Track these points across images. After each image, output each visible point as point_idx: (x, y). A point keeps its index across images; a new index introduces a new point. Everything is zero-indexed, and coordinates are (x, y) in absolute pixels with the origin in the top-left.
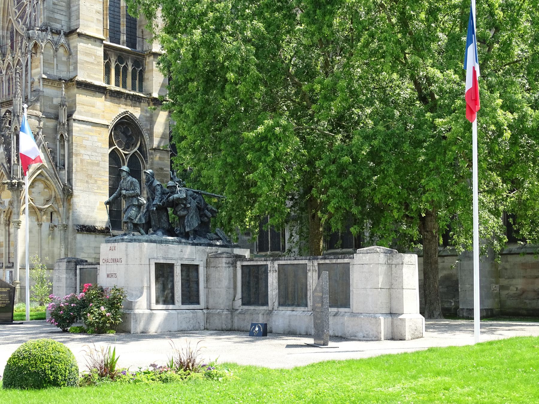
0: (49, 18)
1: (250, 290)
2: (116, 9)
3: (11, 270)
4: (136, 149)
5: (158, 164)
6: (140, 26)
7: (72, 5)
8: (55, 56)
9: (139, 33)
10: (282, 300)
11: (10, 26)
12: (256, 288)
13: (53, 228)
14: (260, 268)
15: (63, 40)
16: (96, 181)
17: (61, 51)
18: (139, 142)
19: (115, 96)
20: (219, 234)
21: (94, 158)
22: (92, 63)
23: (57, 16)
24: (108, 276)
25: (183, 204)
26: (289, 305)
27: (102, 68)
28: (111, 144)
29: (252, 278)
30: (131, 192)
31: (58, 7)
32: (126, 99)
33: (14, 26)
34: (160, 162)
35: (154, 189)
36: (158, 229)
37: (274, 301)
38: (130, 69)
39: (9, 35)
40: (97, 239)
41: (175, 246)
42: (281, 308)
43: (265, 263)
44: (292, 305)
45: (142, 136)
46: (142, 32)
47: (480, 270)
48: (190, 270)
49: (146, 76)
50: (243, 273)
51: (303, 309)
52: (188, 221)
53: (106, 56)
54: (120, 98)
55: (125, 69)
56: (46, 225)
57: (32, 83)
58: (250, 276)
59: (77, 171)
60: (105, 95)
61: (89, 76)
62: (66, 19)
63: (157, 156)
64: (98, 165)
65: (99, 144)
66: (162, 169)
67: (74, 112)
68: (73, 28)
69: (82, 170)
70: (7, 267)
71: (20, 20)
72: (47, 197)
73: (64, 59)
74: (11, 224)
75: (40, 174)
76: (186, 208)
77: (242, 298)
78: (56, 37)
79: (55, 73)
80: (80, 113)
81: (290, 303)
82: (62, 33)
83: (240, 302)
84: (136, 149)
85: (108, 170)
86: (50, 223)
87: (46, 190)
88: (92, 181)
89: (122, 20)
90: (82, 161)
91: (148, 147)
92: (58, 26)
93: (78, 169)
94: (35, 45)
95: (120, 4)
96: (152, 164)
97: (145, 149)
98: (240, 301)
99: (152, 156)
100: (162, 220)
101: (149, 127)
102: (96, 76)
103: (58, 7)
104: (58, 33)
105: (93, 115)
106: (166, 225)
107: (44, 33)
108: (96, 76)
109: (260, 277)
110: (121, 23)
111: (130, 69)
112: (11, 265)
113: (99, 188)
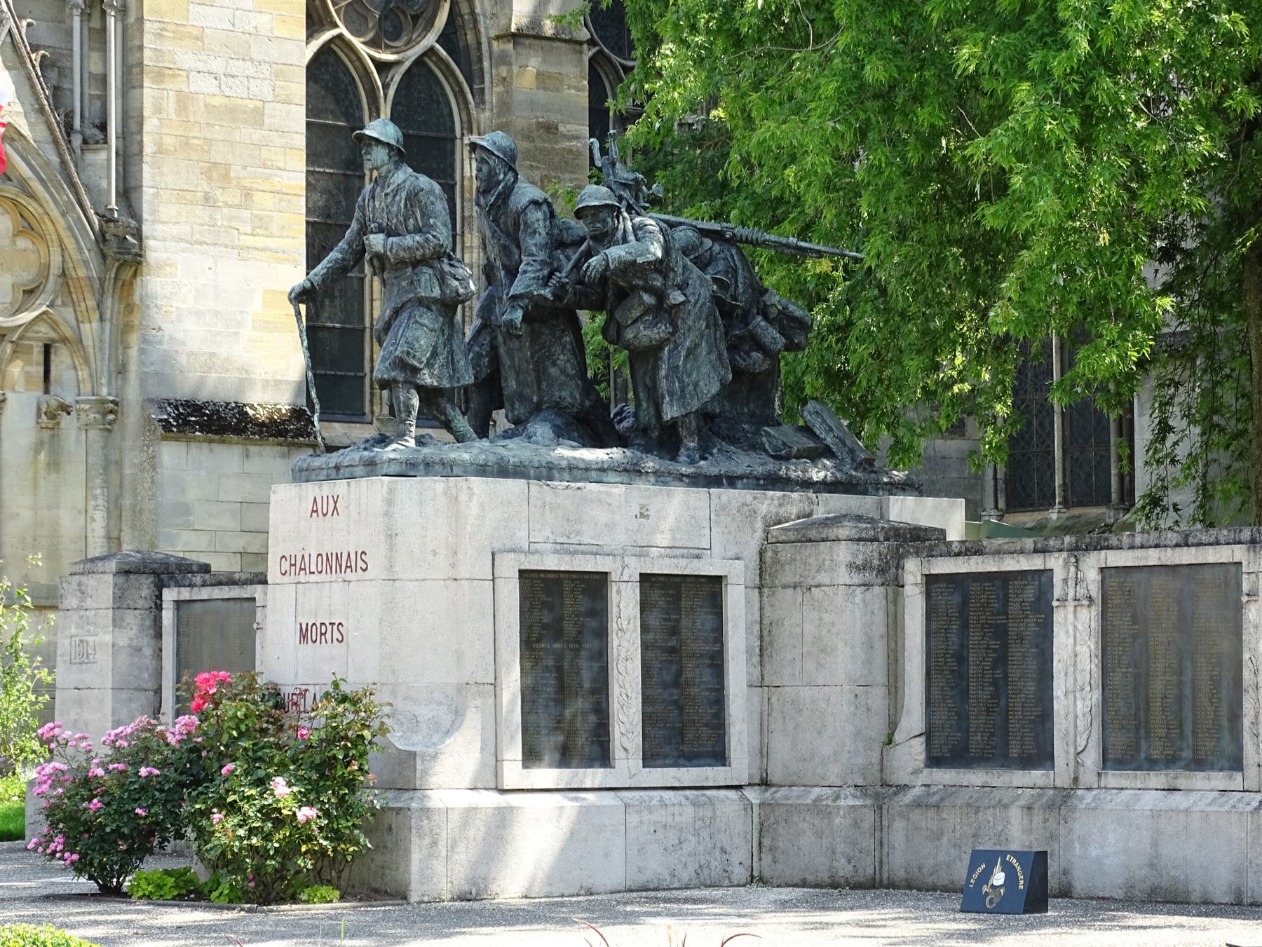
1: (965, 694)
4: (431, 39)
5: (532, 104)
10: (1119, 740)
12: (995, 683)
13: (52, 416)
14: (1014, 585)
24: (304, 636)
26: (1152, 764)
29: (974, 637)
30: (409, 240)
34: (542, 96)
35: (517, 225)
37: (1081, 743)
42: (1114, 778)
43: (1036, 563)
44: (1170, 762)
48: (681, 601)
50: (931, 613)
51: (1218, 780)
52: (674, 369)
58: (965, 626)
59: (160, 150)
63: (528, 70)
66: (549, 129)
72: (27, 277)
76: (663, 310)
77: (929, 734)
81: (1156, 754)
84: (431, 39)
87: (23, 243)
88: (233, 196)
91: (488, 29)
93: (169, 142)
97: (470, 37)
98: (919, 746)
99: (503, 71)
100: (553, 371)
106: (569, 394)
109: (1013, 630)
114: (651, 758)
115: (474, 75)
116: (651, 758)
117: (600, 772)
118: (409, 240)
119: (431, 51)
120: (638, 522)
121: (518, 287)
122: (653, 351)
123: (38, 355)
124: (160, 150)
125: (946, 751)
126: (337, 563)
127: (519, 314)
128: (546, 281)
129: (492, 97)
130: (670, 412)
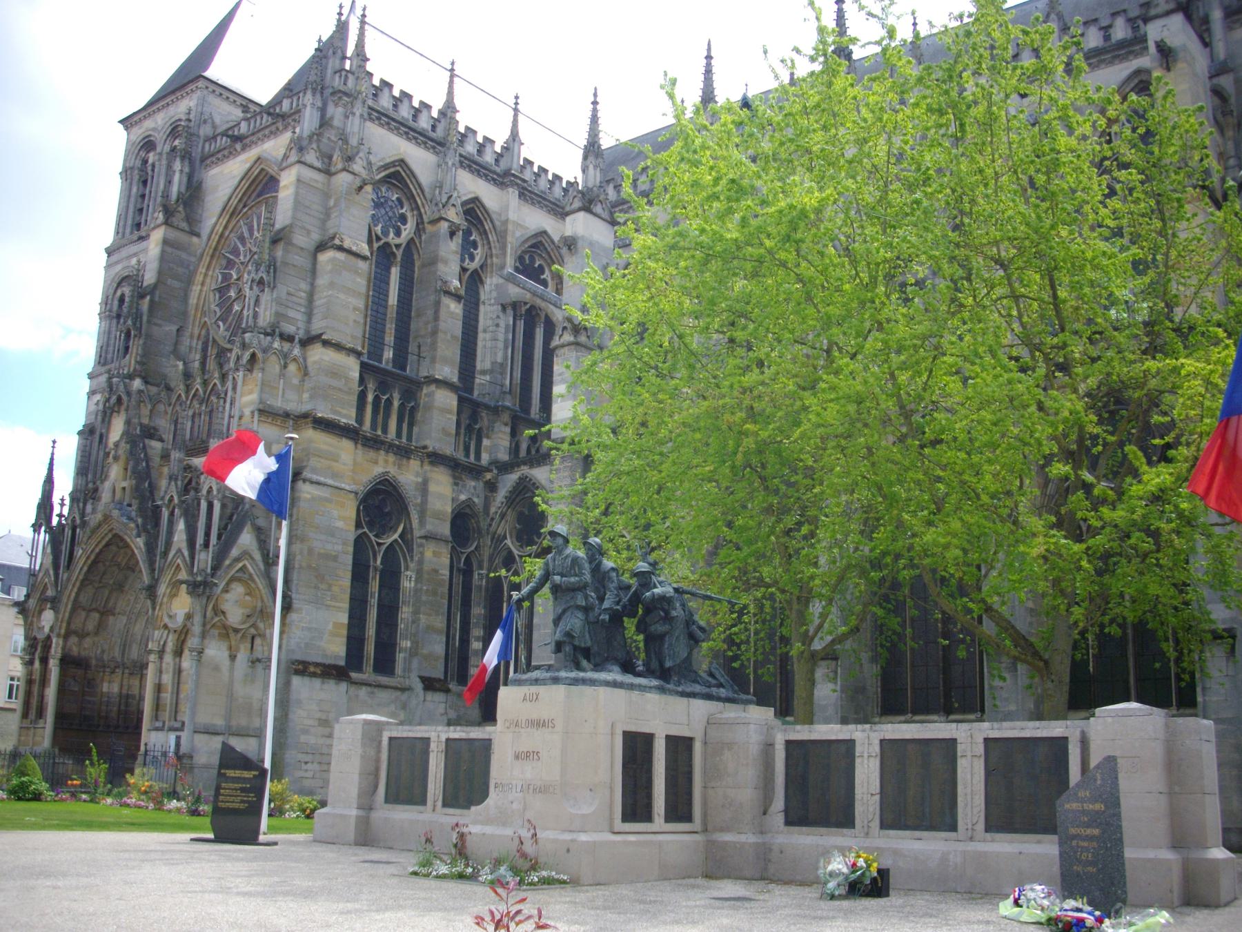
0: (277, 314)
2: (381, 310)
3: (178, 733)
4: (396, 536)
6: (416, 337)
7: (316, 297)
8: (282, 375)
9: (412, 348)
11: (203, 332)
13: (253, 662)
15: (297, 351)
16: (330, 586)
17: (292, 367)
18: (402, 526)
19: (373, 443)
20: (718, 676)
21: (329, 547)
22: (340, 390)
23: (291, 313)
24: (517, 757)
25: (663, 610)
27: (354, 399)
28: (358, 525)
30: (572, 579)
31: (294, 299)
32: (387, 452)
33: (211, 332)
34: (435, 560)
35: (604, 578)
36: (607, 660)
37: (870, 817)
38: (396, 404)
39: (200, 347)
40: (326, 686)
41: (653, 697)
45: (408, 515)
46: (419, 347)
47: (667, 768)
48: (680, 747)
49: (419, 416)
52: (671, 645)
53: (362, 380)
54: (378, 449)
55: (389, 402)
56: (243, 656)
57: (241, 418)
59: (301, 567)
60: (356, 443)
61: (335, 412)
62: (304, 318)
64: (335, 558)
65: (340, 524)
66: (436, 571)
67: (303, 468)
68: (314, 333)
69: (309, 567)
70: (172, 729)
71: (221, 323)
72: (247, 611)
73: (295, 381)
74: (186, 653)
75: (241, 569)
76: (668, 618)
77: (787, 811)
78: (287, 346)
79: (278, 403)
80: (314, 471)
82: (297, 340)
83: (780, 819)
84: (396, 536)
85: (350, 568)
86: (248, 652)
87: (248, 598)
88: (323, 586)
89: (388, 326)
90: (310, 551)
91: (417, 533)
92: (289, 329)
93: (304, 564)
94: (253, 355)
95: (387, 301)
96: (421, 562)
100: (615, 643)
101: (419, 501)
102: (344, 412)
103: (294, 299)
104: (290, 339)
105: (335, 476)
106: (620, 655)
107: (269, 338)
108: (344, 412)
110: (388, 331)
111: (396, 404)
112: (177, 725)
113: (334, 598)
114: (668, 819)
115: (411, 550)
116: (668, 819)
117: (649, 825)
118: (572, 579)
119: (396, 541)
120: (664, 714)
121: (606, 605)
122: (661, 637)
123: (249, 640)
124: (301, 567)
125: (394, 797)
126: (539, 724)
127: (607, 617)
128: (618, 603)
129: (416, 558)
130: (668, 664)
